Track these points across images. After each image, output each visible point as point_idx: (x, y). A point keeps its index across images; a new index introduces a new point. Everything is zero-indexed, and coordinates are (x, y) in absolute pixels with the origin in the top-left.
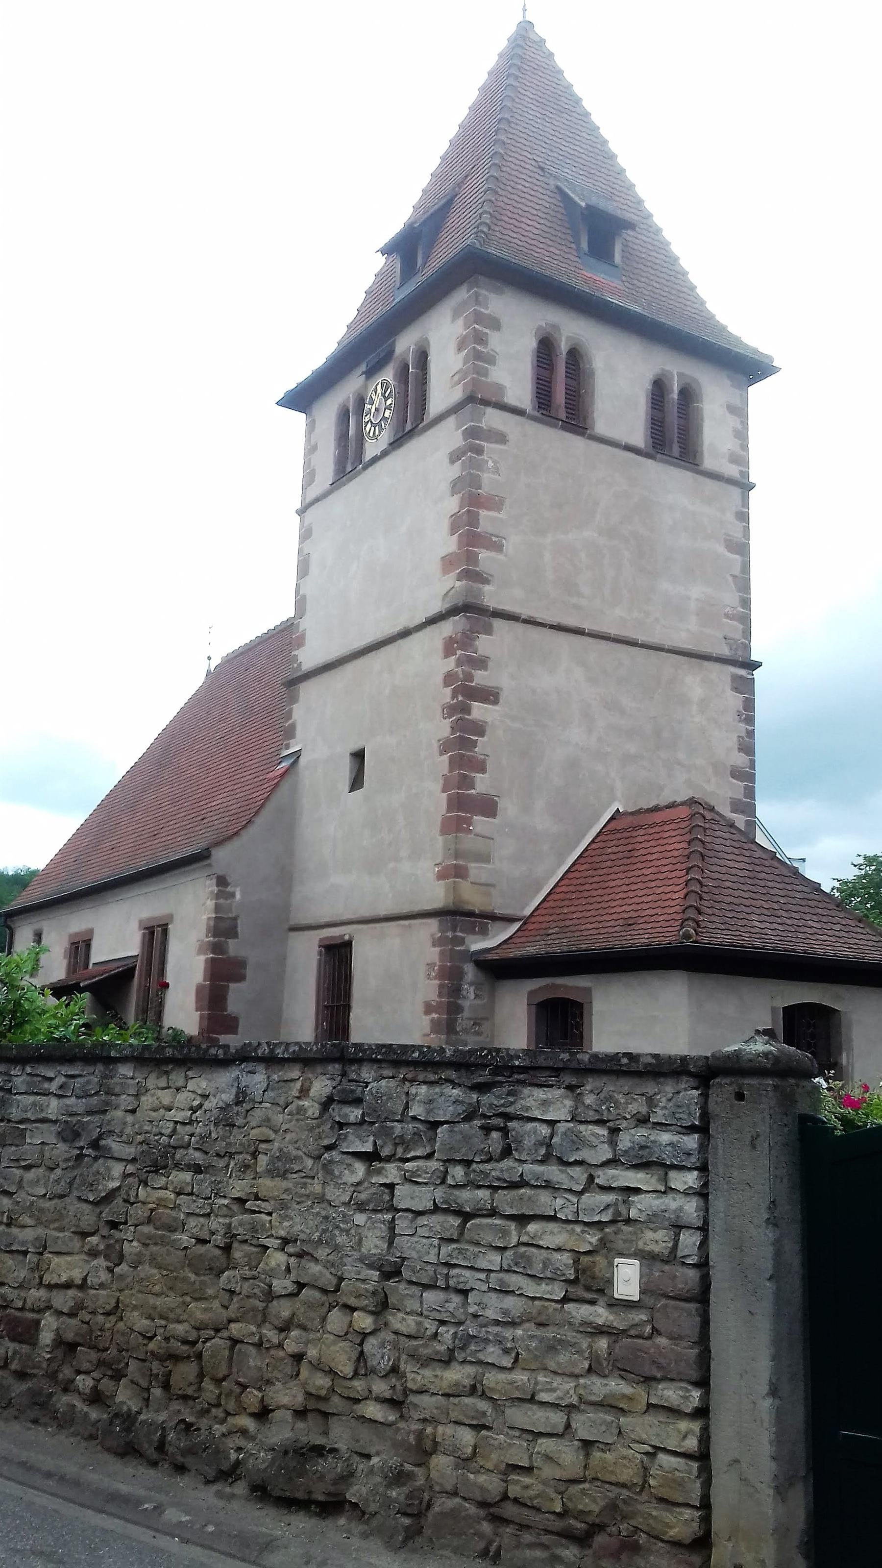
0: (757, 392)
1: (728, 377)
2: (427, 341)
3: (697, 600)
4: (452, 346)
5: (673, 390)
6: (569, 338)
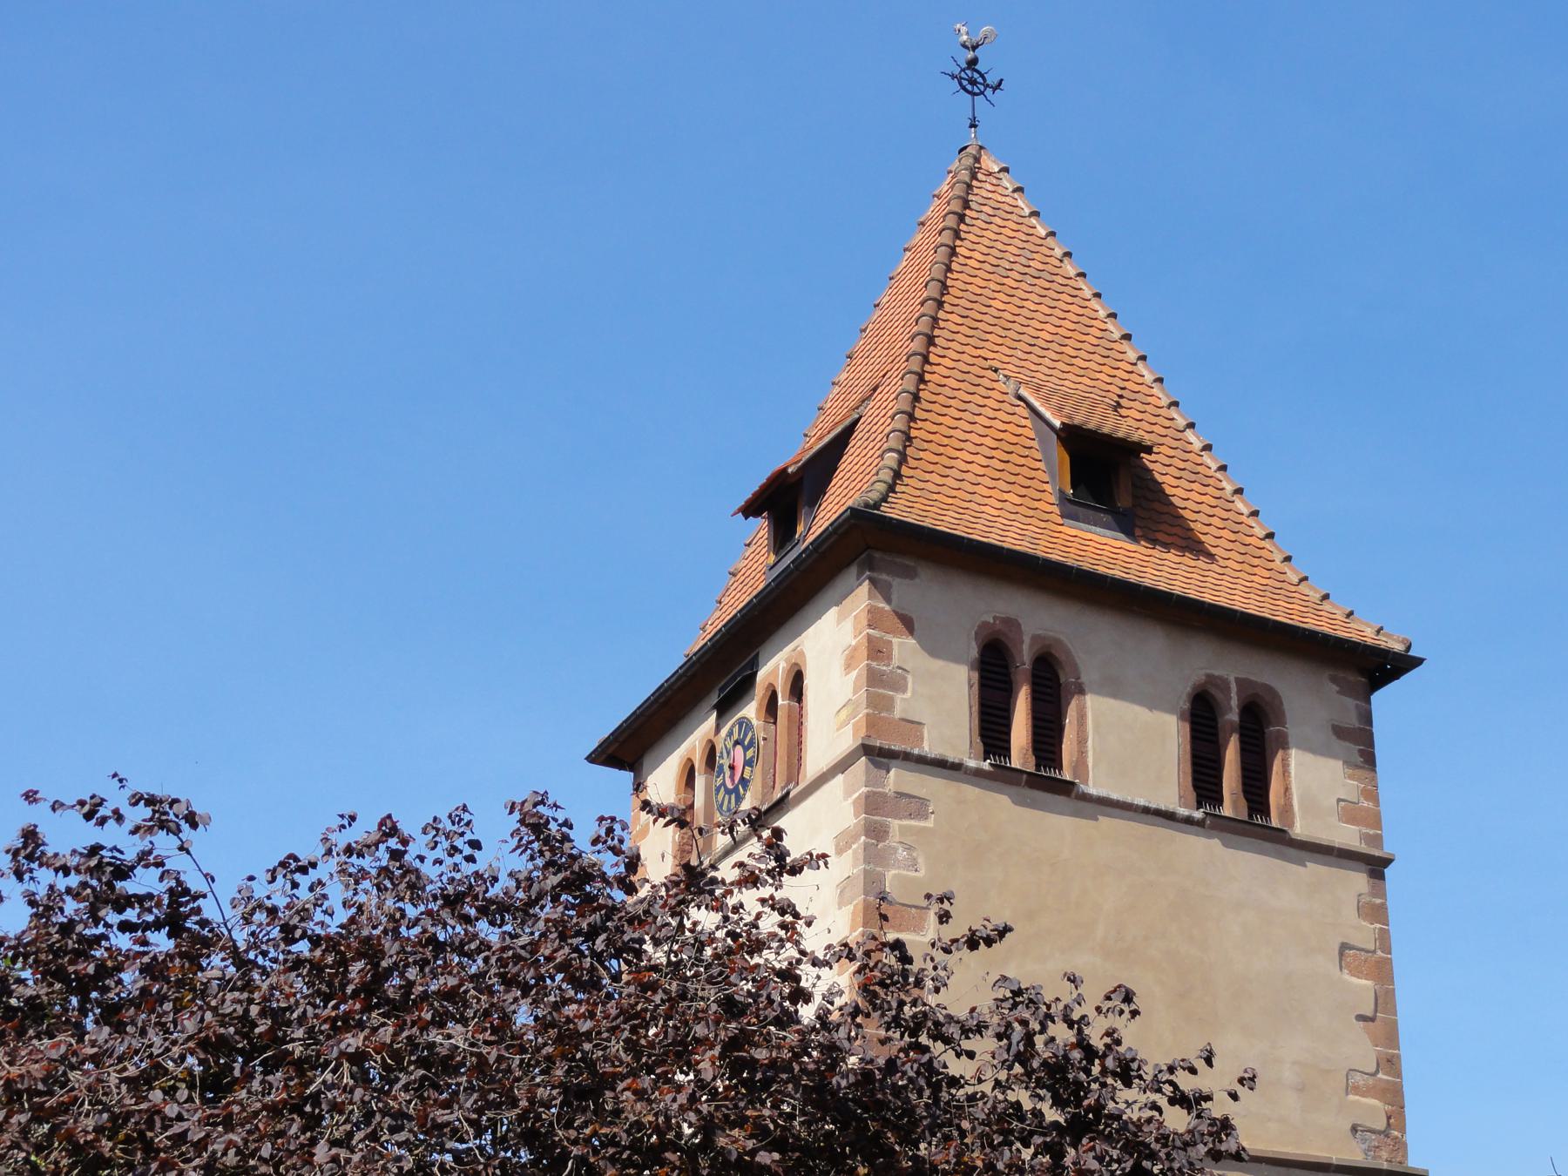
0: (1385, 701)
1: (1334, 680)
2: (802, 654)
3: (1294, 1063)
4: (838, 662)
5: (1231, 708)
6: (1035, 638)
